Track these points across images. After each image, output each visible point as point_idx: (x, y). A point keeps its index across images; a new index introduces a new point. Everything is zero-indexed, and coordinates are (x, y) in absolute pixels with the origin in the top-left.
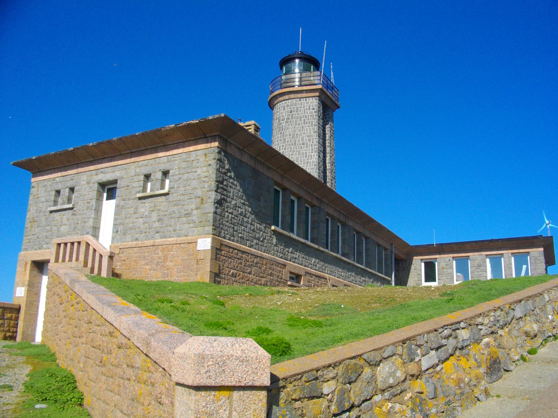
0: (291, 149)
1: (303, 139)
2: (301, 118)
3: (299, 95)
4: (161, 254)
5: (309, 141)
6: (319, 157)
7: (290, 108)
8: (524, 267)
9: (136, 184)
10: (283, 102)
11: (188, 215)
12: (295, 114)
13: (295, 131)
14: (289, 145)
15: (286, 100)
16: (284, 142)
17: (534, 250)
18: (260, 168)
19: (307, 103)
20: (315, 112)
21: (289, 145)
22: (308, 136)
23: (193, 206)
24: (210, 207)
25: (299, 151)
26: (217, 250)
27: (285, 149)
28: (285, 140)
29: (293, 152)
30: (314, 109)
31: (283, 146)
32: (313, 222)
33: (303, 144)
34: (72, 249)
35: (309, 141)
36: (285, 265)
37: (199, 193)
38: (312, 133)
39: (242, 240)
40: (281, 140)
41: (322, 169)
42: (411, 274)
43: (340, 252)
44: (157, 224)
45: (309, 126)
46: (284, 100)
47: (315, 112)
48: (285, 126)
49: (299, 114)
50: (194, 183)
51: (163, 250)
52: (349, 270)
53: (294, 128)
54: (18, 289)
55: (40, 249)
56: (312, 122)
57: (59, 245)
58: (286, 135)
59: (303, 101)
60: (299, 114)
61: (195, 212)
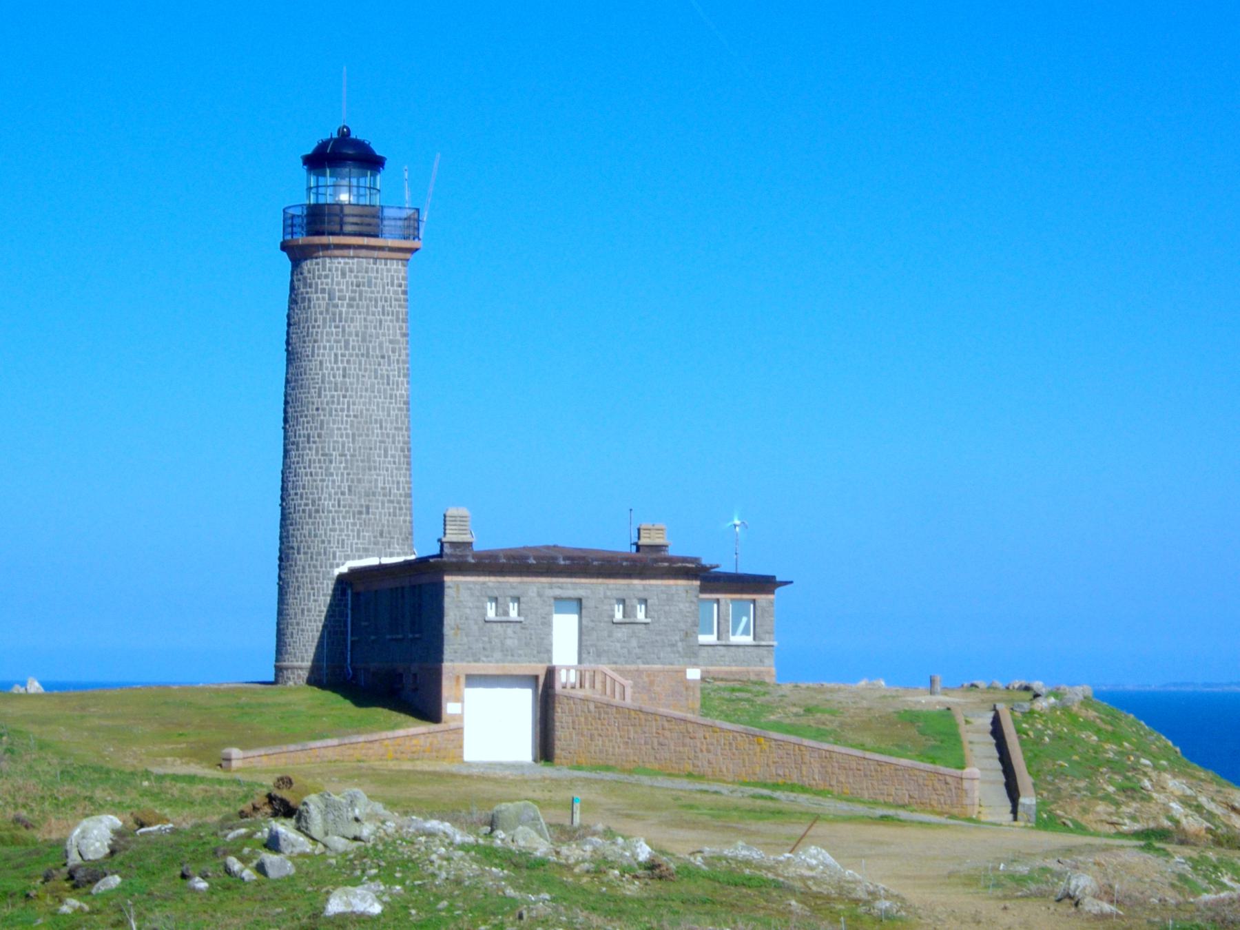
0: (360, 363)
2: (376, 301)
3: (376, 254)
4: (646, 679)
7: (356, 277)
8: (744, 619)
10: (342, 261)
11: (673, 645)
13: (366, 327)
14: (357, 355)
15: (349, 257)
16: (346, 348)
17: (763, 596)
19: (389, 271)
21: (357, 355)
22: (391, 342)
23: (677, 638)
25: (376, 371)
27: (348, 362)
28: (347, 342)
29: (366, 370)
30: (400, 286)
31: (343, 355)
33: (383, 357)
37: (682, 626)
38: (398, 337)
44: (637, 650)
45: (392, 321)
46: (343, 257)
48: (347, 313)
49: (372, 292)
51: (648, 676)
53: (365, 320)
55: (475, 661)
56: (398, 312)
58: (350, 334)
59: (381, 265)
60: (372, 292)
61: (680, 644)
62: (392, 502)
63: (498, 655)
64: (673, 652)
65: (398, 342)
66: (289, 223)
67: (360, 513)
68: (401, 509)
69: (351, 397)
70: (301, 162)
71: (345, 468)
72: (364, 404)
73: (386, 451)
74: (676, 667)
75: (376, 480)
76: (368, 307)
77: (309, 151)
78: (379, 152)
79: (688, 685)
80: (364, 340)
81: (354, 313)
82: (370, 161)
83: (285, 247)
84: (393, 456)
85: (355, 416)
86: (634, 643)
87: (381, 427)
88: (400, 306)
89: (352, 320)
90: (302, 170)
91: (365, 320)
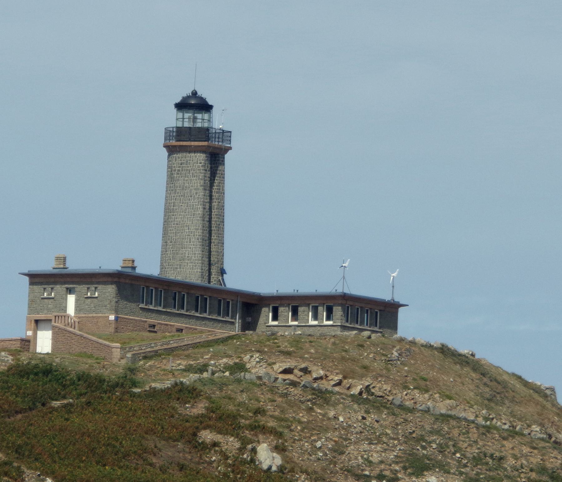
0: (180, 200)
1: (191, 192)
5: (196, 194)
6: (204, 208)
9: (83, 291)
12: (185, 167)
14: (179, 196)
18: (133, 282)
20: (202, 166)
21: (179, 196)
24: (113, 303)
25: (188, 203)
26: (117, 319)
30: (201, 163)
32: (164, 297)
33: (191, 196)
34: (61, 320)
35: (196, 194)
36: (146, 322)
37: (109, 298)
39: (126, 314)
40: (172, 190)
41: (207, 219)
42: (261, 315)
43: (76, 328)
44: (93, 308)
47: (202, 166)
50: (107, 294)
52: (190, 319)
54: (113, 319)
57: (55, 316)
62: (192, 263)
63: (46, 311)
64: (106, 309)
65: (198, 189)
66: (168, 134)
67: (177, 268)
68: (195, 266)
69: (175, 215)
70: (174, 107)
71: (172, 248)
72: (181, 218)
73: (190, 239)
74: (106, 315)
75: (185, 253)
76: (185, 174)
77: (178, 100)
78: (210, 103)
79: (110, 322)
80: (183, 189)
81: (179, 177)
82: (205, 107)
83: (164, 147)
84: (193, 242)
85: (177, 224)
86: (92, 305)
87: (189, 229)
88: (200, 173)
89: (178, 180)
90: (175, 110)
91: (184, 180)
